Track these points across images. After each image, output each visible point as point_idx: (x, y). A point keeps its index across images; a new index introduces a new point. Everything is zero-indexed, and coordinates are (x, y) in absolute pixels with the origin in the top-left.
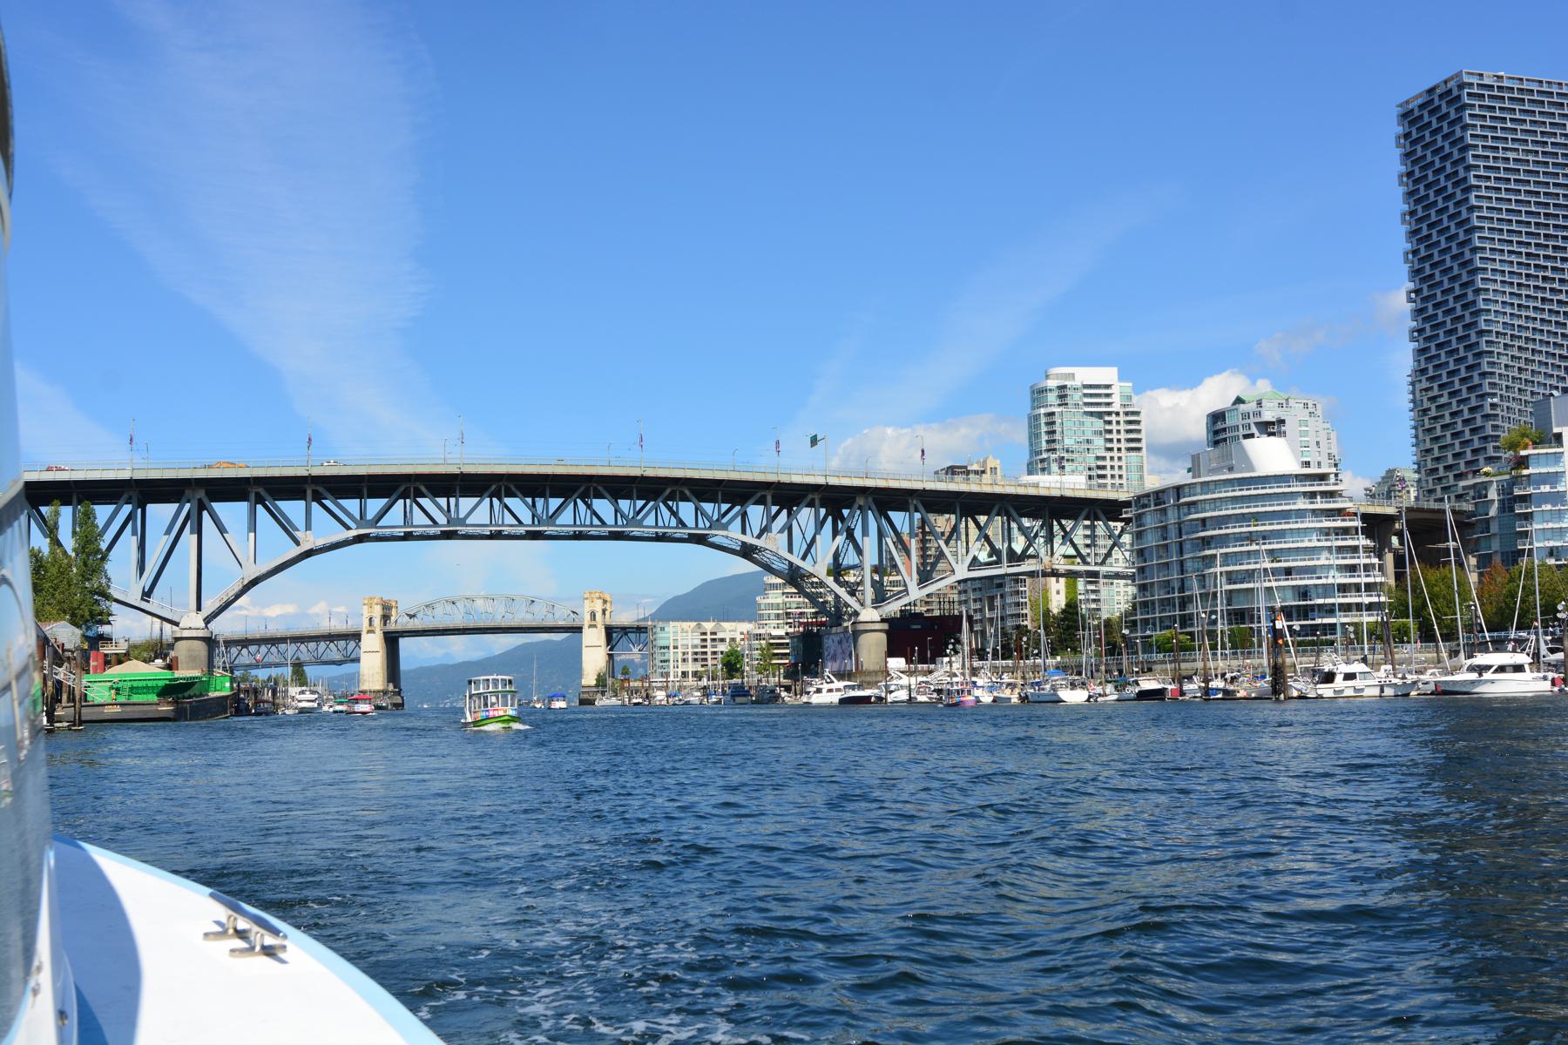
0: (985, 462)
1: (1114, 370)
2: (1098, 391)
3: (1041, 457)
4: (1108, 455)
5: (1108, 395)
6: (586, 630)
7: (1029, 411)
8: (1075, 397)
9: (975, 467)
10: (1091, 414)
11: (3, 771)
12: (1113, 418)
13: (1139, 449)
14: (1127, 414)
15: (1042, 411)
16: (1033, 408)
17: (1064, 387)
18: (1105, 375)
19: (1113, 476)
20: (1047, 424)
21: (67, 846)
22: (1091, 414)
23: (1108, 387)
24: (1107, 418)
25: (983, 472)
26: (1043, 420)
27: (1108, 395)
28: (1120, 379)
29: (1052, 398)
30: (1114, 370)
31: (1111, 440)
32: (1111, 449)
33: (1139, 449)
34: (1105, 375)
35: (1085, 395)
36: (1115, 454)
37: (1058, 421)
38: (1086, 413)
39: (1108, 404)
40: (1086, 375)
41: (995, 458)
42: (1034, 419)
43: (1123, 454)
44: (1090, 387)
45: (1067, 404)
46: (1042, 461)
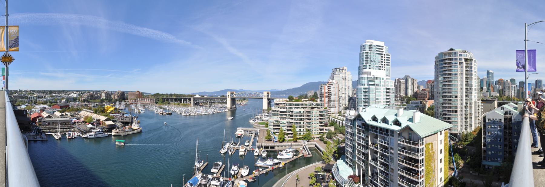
0: (344, 67)
1: (383, 43)
2: (379, 47)
3: (363, 65)
4: (382, 66)
5: (382, 49)
6: (264, 99)
7: (359, 52)
8: (374, 49)
9: (341, 69)
10: (378, 54)
11: (1, 159)
12: (383, 56)
13: (389, 65)
14: (387, 55)
15: (365, 52)
16: (361, 51)
17: (371, 45)
18: (381, 44)
19: (383, 67)
20: (366, 55)
21: (291, 87)
22: (378, 54)
23: (382, 47)
24: (382, 56)
25: (343, 70)
26: (365, 54)
27: (382, 49)
28: (385, 45)
29: (367, 48)
30: (383, 43)
31: (382, 59)
32: (382, 64)
33: (389, 65)
34: (381, 44)
35: (377, 48)
36: (384, 66)
37: (369, 55)
38: (377, 53)
39: (382, 52)
40: (376, 43)
41: (346, 67)
42: (361, 55)
43: (386, 66)
44: (378, 46)
45: (372, 50)
46: (364, 66)
